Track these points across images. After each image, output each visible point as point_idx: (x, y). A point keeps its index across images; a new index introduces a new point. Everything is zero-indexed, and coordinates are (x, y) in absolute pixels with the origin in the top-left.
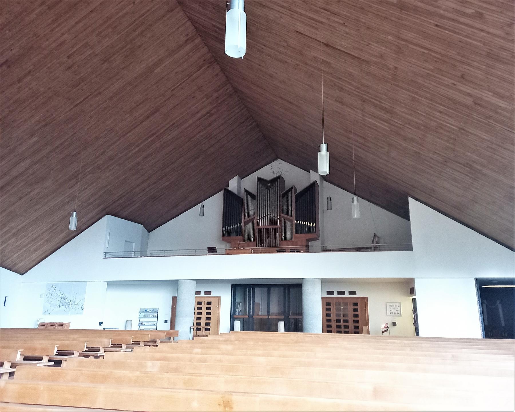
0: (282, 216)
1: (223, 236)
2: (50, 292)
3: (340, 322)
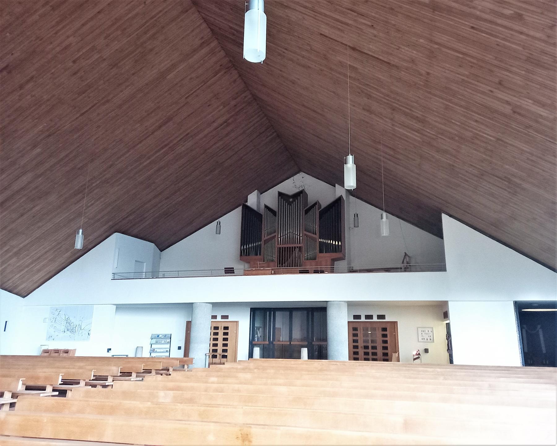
0: (305, 234)
1: (241, 255)
2: (54, 316)
3: (367, 349)
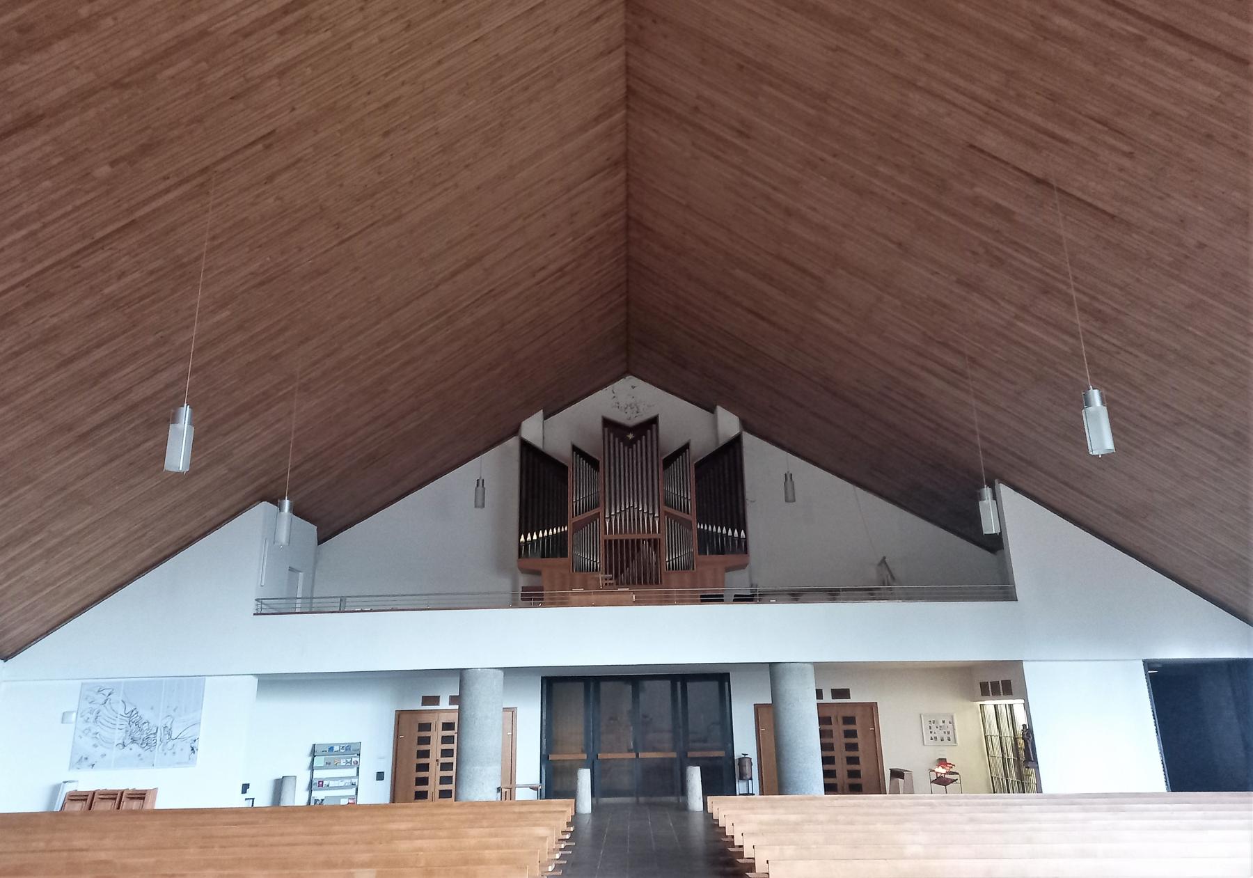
2: (93, 706)
